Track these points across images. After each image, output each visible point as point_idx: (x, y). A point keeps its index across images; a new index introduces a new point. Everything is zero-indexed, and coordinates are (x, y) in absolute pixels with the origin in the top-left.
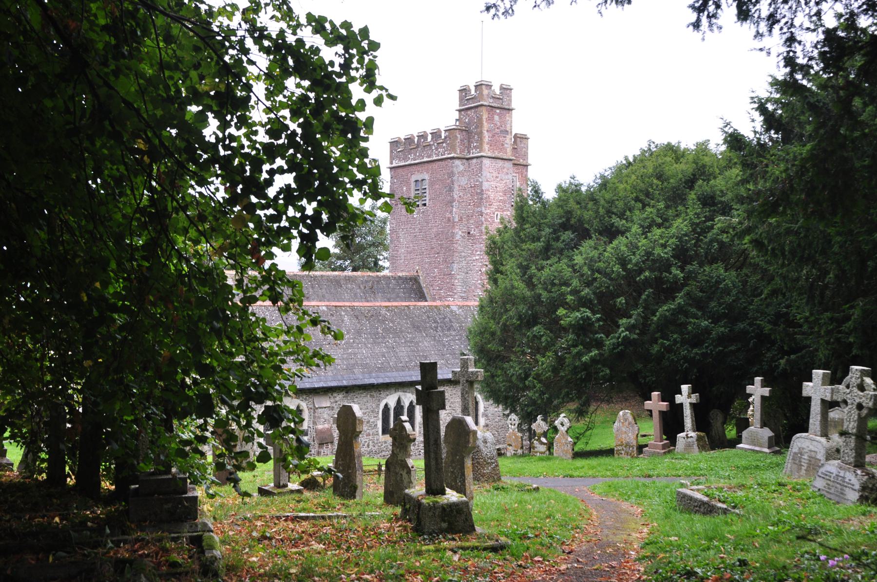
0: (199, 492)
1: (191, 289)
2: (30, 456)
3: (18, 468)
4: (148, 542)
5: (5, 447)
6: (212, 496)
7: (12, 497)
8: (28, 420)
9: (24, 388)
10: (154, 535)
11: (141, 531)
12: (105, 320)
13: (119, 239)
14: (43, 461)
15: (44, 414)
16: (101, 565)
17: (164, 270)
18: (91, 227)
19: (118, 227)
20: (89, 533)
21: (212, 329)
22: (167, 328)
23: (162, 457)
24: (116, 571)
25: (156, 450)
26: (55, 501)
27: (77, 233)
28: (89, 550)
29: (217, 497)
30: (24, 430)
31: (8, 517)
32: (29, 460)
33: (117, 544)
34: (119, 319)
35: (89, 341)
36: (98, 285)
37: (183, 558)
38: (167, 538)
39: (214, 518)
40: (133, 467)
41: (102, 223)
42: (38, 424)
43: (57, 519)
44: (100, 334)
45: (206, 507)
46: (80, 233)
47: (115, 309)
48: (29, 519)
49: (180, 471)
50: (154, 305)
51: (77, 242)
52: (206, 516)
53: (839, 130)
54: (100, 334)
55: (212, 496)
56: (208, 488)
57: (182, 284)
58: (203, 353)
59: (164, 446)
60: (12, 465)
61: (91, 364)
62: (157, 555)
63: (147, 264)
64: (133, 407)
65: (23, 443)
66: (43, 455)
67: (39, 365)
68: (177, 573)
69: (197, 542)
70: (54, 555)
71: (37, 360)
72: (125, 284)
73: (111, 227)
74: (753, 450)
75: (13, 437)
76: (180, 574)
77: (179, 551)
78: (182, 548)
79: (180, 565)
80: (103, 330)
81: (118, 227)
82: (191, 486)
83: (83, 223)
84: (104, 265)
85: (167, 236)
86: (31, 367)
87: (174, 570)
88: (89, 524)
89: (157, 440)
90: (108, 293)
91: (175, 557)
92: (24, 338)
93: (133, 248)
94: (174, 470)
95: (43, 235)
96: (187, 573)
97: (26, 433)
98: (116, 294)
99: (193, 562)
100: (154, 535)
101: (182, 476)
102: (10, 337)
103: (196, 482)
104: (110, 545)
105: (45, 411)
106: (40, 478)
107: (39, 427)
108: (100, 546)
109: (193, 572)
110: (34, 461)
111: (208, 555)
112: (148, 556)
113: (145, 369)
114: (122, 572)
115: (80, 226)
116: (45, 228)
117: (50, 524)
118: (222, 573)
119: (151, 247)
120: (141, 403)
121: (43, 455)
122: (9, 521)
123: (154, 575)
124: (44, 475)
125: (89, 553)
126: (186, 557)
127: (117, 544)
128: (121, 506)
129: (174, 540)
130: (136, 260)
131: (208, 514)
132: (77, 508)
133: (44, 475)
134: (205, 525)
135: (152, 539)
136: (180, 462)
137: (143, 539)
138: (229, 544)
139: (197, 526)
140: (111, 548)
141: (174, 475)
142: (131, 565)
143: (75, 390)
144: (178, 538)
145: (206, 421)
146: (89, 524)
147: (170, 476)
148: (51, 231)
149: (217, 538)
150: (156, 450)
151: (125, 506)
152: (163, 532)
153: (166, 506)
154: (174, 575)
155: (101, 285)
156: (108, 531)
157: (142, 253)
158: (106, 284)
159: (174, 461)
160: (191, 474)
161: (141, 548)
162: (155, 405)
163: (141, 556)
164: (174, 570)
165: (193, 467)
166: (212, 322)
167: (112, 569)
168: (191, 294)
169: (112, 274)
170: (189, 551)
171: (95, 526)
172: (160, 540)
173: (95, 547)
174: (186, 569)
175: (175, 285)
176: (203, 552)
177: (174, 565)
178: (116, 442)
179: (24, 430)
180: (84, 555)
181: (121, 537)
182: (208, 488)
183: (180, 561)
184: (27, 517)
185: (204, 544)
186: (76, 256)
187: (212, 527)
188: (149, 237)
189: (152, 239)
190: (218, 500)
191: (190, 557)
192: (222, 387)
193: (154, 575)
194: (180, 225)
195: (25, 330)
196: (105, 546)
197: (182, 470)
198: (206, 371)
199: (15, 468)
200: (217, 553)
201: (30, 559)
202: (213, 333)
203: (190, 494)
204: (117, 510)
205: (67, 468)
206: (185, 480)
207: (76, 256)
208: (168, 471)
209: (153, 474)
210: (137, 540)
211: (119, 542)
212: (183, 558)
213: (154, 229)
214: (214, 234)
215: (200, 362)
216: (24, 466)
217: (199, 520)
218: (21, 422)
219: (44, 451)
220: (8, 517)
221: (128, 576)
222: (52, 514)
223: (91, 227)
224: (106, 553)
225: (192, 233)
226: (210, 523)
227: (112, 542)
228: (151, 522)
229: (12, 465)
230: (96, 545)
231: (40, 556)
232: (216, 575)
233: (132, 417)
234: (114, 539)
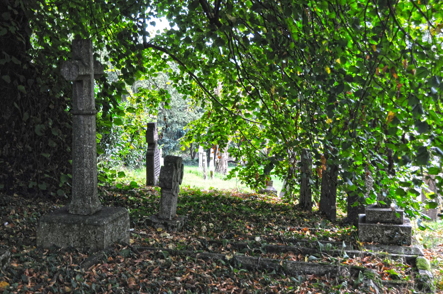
0: (413, 224)
1: (412, 61)
2: (288, 187)
3: (280, 194)
4: (374, 257)
5: (272, 180)
6: (423, 228)
7: (278, 214)
8: (286, 161)
9: (284, 138)
10: (378, 253)
11: (367, 248)
12: (342, 88)
13: (355, 23)
14: (296, 191)
15: (297, 157)
16: (341, 268)
17: (391, 47)
18: (334, 16)
19: (355, 15)
20: (331, 245)
21: (430, 94)
22: (392, 94)
23: (384, 194)
24: (352, 275)
25: (379, 188)
26: (305, 220)
27: (323, 22)
28: (332, 257)
29: (426, 230)
30: (284, 168)
31: (276, 227)
32: (288, 190)
33: (351, 255)
34: (355, 87)
35: (331, 104)
36: (338, 61)
37: (401, 273)
38: (388, 256)
39: (425, 246)
40: (362, 200)
41: (342, 12)
42: (293, 164)
43: (308, 233)
44: (340, 99)
45: (417, 236)
46: (326, 21)
47: (350, 79)
48: (290, 230)
49: (398, 206)
50: (382, 76)
51: (323, 29)
52: (418, 243)
53: (370, 73)
54: (340, 99)
55: (423, 228)
56: (420, 222)
57: (405, 58)
58: (422, 113)
59: (385, 186)
60: (276, 192)
61: (331, 122)
62: (381, 268)
63: (376, 43)
64: (363, 154)
65: (284, 177)
66: (296, 187)
67: (294, 122)
68: (397, 284)
69: (412, 261)
70: (308, 257)
71: (293, 118)
72: (358, 59)
73: (349, 15)
74: (397, 224)
75: (277, 172)
76: (399, 284)
77: (398, 267)
78: (400, 265)
79: (399, 278)
80: (342, 95)
81: (355, 15)
82: (407, 218)
83: (328, 13)
84: (343, 44)
85: (394, 18)
86: (289, 123)
87: (394, 281)
88: (330, 239)
89: (380, 181)
90: (345, 67)
91: (394, 271)
92: (284, 101)
93: (367, 31)
94: (393, 205)
95: (299, 25)
96: (405, 285)
97: (285, 170)
98: (352, 68)
99: (410, 277)
100: (378, 253)
101: (399, 210)
102: (275, 102)
103: (411, 216)
104: (346, 255)
105: (298, 156)
106: (294, 203)
107: (294, 167)
108: (339, 255)
109: (410, 285)
110: (291, 190)
111: (421, 273)
112: (374, 267)
113: (374, 125)
114: (356, 277)
115: (325, 17)
116: (301, 19)
117: (303, 235)
118: (434, 289)
119: (382, 28)
120: (370, 152)
121: (296, 187)
122: (277, 230)
123: (380, 282)
124: (297, 201)
125: (331, 259)
126: (404, 272)
127: (351, 255)
128: (352, 229)
129: (394, 258)
130: (368, 40)
131: (419, 242)
132: (321, 226)
133: (297, 201)
134: (417, 250)
135: (377, 255)
136: (398, 199)
137: (370, 255)
138: (438, 268)
139: (410, 250)
140: (347, 258)
141: (393, 209)
142: (363, 271)
143: (319, 141)
144: (397, 257)
145: (422, 169)
146: (330, 239)
147: (390, 210)
148: (305, 21)
149: (428, 262)
150: (379, 188)
151: (355, 229)
152: (384, 251)
153: (386, 232)
154: (395, 285)
155: (341, 61)
156: (344, 245)
157: (372, 34)
158: (344, 60)
159: (393, 197)
160: (407, 209)
161: (368, 261)
162: (380, 154)
163: (369, 267)
164: (394, 281)
165: (408, 204)
166: (430, 89)
167: (349, 273)
168: (413, 65)
169: (348, 53)
170: (406, 268)
171: (334, 241)
172: (383, 257)
173: (335, 256)
174: (404, 282)
175: (399, 59)
176: (417, 270)
177: (394, 277)
178: (351, 180)
179: (284, 168)
180: (328, 260)
181: (353, 251)
182: (420, 222)
183: (399, 275)
184: (289, 229)
185: (418, 264)
186: (322, 39)
187: (423, 253)
188: (379, 20)
189: (381, 22)
190: (427, 233)
191: (407, 273)
192: (437, 142)
193: (380, 282)
194: (405, 9)
195: (285, 96)
196: (342, 256)
197: (399, 205)
198: (423, 127)
199: (278, 194)
200: (429, 273)
201: (293, 258)
202: (431, 97)
203: (405, 225)
204: (349, 231)
205: (313, 198)
206: (401, 213)
207: (322, 39)
208: (388, 206)
209: (376, 207)
210: (365, 255)
211: (353, 254)
212: (401, 273)
213: (383, 14)
214: (434, 14)
215: (419, 120)
216: (284, 194)
217: (412, 246)
218: (282, 162)
219: (297, 184)
220: (276, 227)
221: (361, 280)
222: (304, 228)
223: (334, 16)
224: (343, 261)
225: (415, 15)
226: (421, 248)
227: (348, 253)
228: (374, 242)
229: (276, 192)
230: (336, 254)
231: (299, 257)
232: (428, 290)
233: (361, 163)
234: (349, 251)
